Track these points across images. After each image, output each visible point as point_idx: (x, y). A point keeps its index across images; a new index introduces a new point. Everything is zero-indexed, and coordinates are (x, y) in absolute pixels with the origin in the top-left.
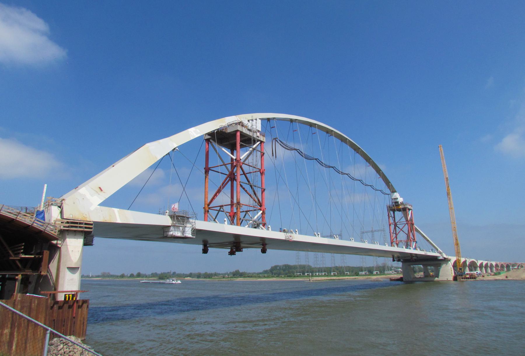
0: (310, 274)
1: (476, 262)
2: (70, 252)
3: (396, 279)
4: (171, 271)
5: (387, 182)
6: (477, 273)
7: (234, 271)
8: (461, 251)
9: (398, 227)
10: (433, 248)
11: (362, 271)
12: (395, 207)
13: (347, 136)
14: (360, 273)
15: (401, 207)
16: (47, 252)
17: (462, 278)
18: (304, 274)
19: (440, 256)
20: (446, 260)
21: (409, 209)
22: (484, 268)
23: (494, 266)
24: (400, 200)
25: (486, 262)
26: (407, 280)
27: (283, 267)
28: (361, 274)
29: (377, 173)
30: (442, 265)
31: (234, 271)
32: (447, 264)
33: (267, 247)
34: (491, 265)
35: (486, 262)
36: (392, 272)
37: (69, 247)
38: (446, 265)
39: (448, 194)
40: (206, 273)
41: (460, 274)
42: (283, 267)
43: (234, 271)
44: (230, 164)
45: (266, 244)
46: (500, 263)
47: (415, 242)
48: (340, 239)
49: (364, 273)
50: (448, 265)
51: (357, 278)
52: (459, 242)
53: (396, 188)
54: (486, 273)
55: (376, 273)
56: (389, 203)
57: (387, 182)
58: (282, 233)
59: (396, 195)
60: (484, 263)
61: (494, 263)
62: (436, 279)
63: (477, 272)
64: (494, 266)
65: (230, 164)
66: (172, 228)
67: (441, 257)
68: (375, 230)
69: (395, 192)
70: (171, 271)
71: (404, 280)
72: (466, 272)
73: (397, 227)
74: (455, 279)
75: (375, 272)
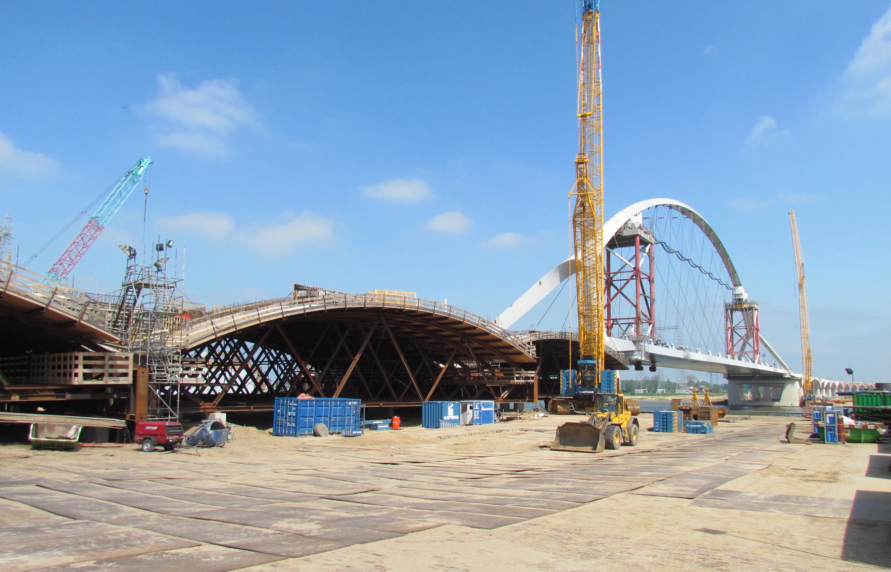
1: (818, 380)
3: (717, 402)
5: (732, 273)
6: (823, 397)
8: (813, 368)
9: (736, 332)
10: (777, 363)
11: (639, 388)
12: (737, 305)
13: (695, 210)
14: (636, 391)
15: (745, 306)
17: (812, 404)
19: (786, 374)
20: (792, 379)
21: (756, 309)
22: (830, 390)
23: (837, 387)
24: (745, 296)
25: (829, 381)
26: (734, 404)
30: (787, 385)
32: (793, 384)
33: (657, 364)
34: (834, 385)
35: (829, 381)
36: (686, 391)
38: (792, 385)
39: (800, 286)
41: (808, 398)
45: (655, 362)
46: (844, 383)
47: (651, 325)
48: (704, 354)
49: (641, 391)
50: (794, 385)
51: (644, 398)
52: (812, 355)
53: (741, 279)
56: (730, 300)
57: (732, 273)
58: (680, 351)
59: (740, 290)
60: (827, 382)
61: (837, 384)
62: (776, 404)
63: (823, 395)
64: (837, 387)
66: (636, 353)
67: (788, 374)
69: (740, 285)
71: (730, 403)
72: (816, 396)
73: (734, 333)
74: (803, 404)
75: (659, 391)
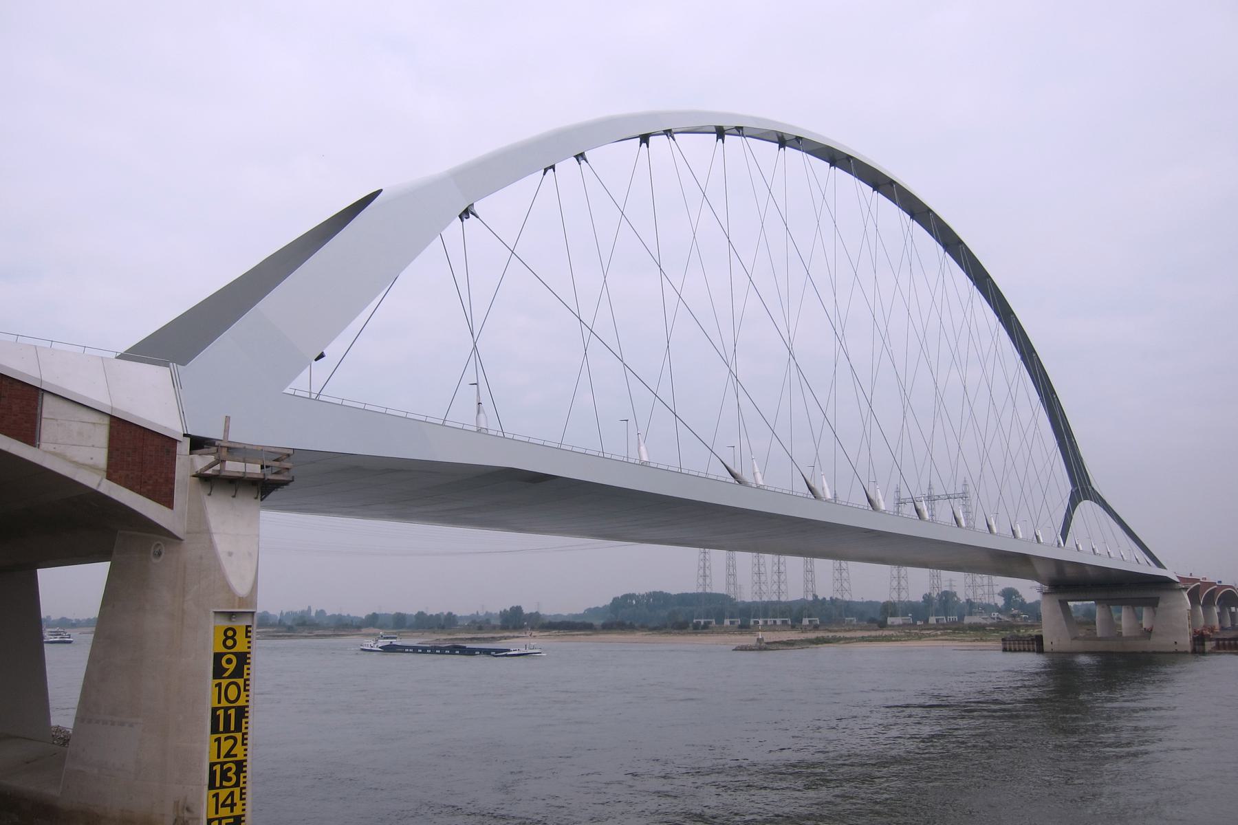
0: (761, 622)
2: (223, 557)
4: (309, 608)
7: (505, 610)
14: (890, 620)
16: (230, 554)
18: (720, 621)
27: (648, 600)
28: (893, 623)
29: (913, 217)
31: (508, 609)
37: (216, 538)
40: (421, 615)
42: (648, 600)
43: (505, 610)
44: (639, 139)
54: (812, 626)
55: (783, 621)
65: (639, 139)
68: (939, 497)
70: (309, 608)
